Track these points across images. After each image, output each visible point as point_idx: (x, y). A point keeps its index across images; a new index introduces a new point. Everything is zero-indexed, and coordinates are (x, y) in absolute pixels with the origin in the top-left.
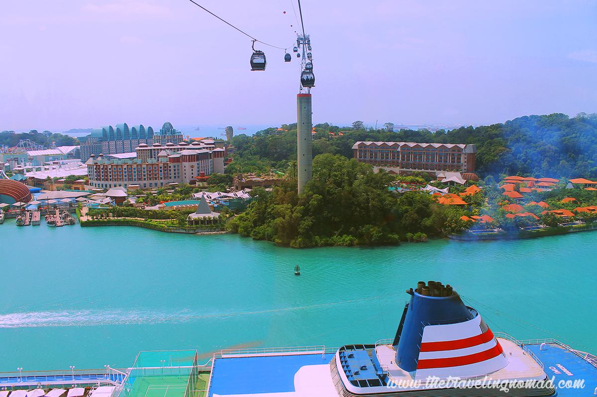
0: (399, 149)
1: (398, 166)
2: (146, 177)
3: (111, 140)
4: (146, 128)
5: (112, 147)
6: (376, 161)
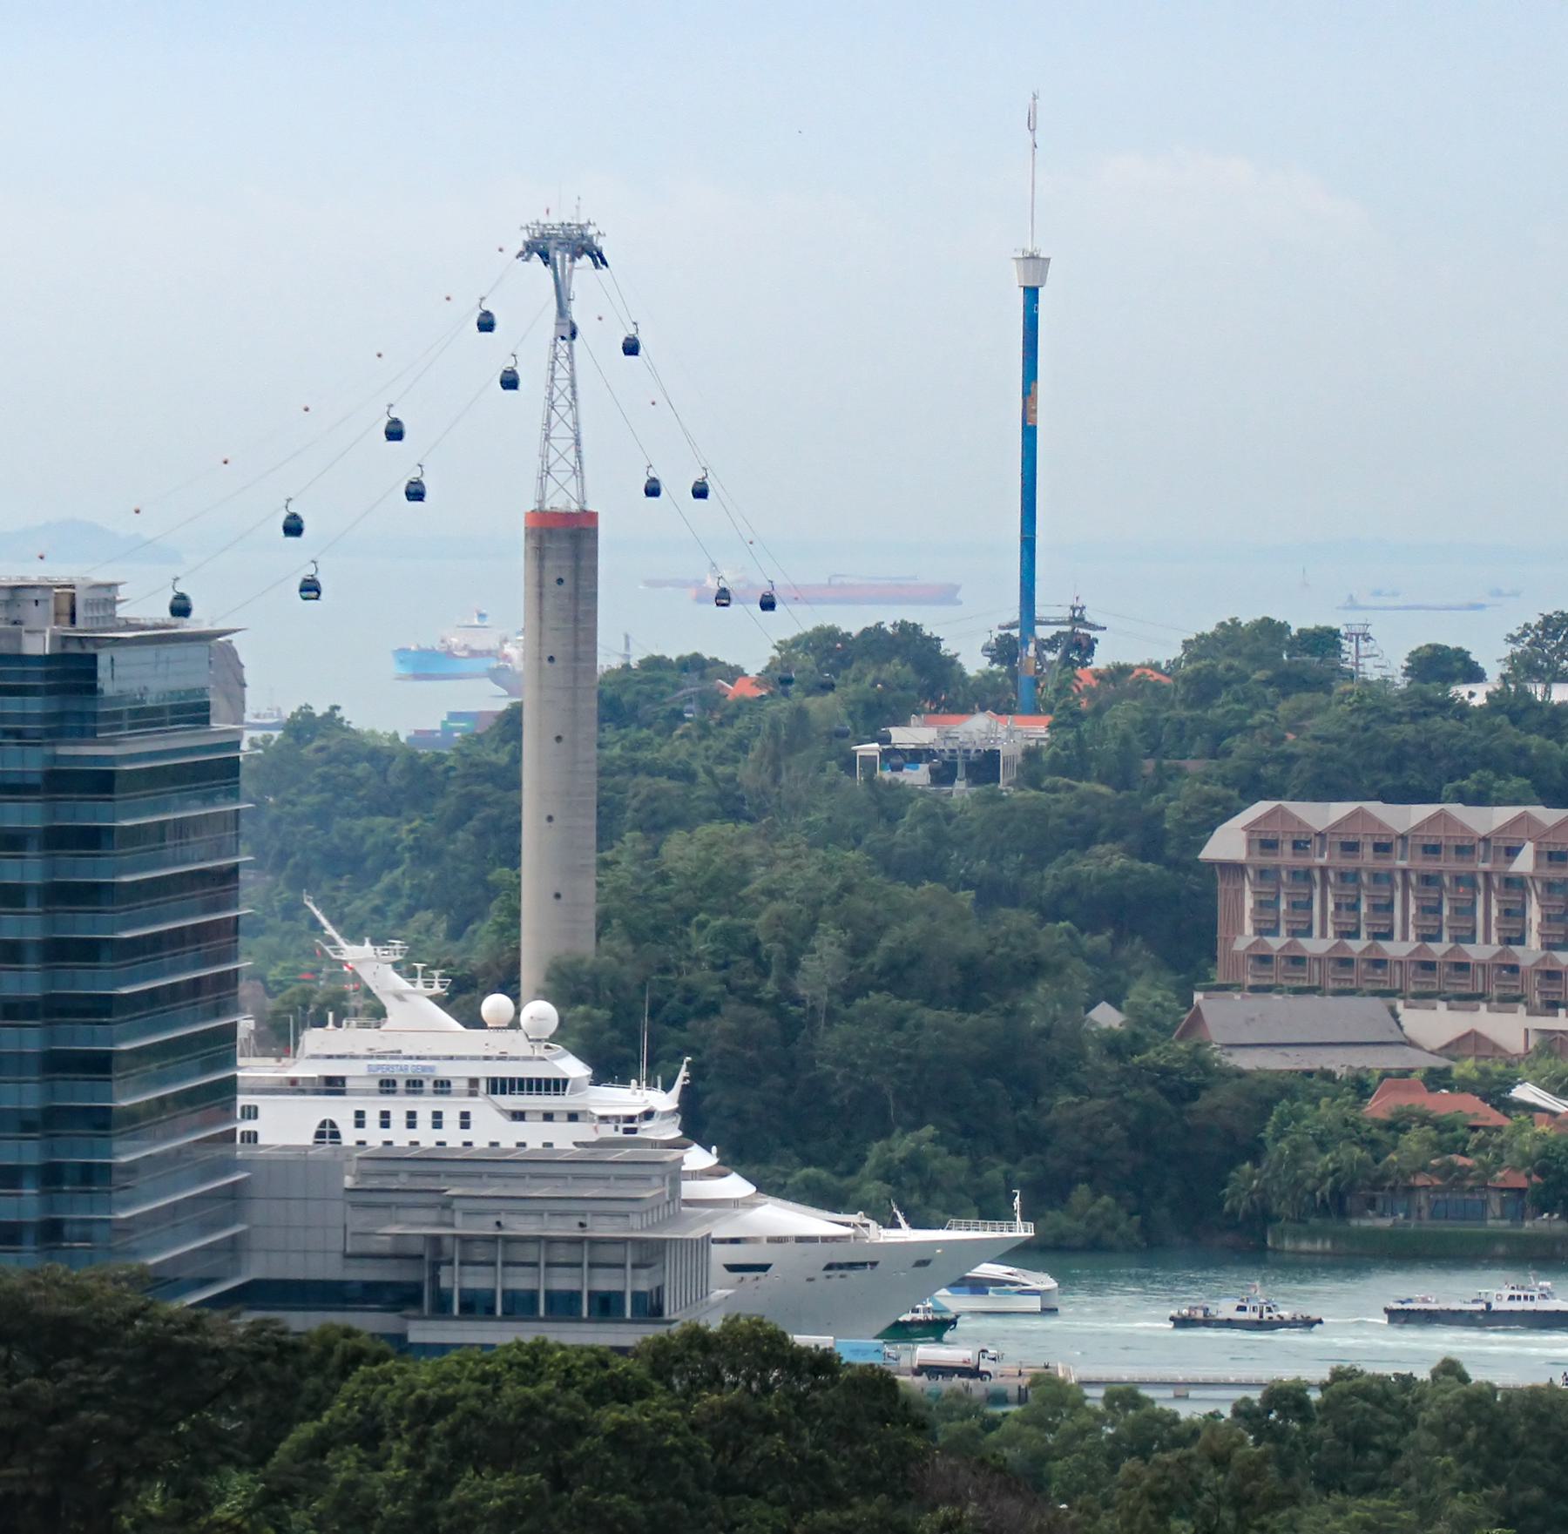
0: (1524, 863)
1: (1509, 1001)
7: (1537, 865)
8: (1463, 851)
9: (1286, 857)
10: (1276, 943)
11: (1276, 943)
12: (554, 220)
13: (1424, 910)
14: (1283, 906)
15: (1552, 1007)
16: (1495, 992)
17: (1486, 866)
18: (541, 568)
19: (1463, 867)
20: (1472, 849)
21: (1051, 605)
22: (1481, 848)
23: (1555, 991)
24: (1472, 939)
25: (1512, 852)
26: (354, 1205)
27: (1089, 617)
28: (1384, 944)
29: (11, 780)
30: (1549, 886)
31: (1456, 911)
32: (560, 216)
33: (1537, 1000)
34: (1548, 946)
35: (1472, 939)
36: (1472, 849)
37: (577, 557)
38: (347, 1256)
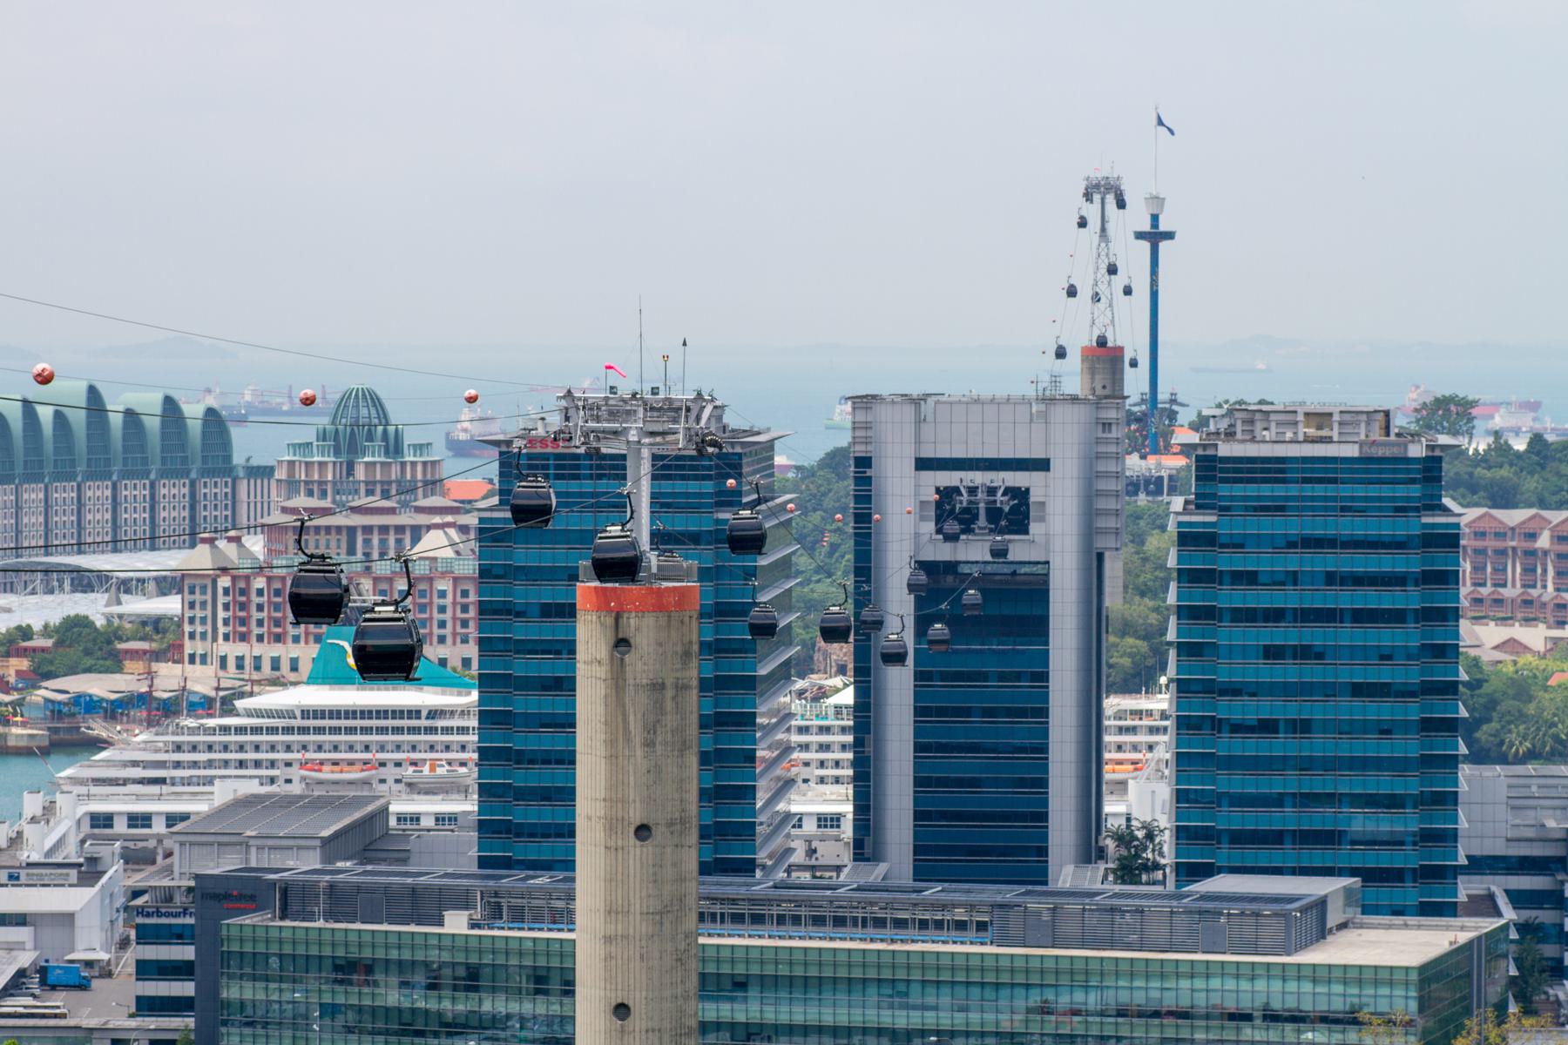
0: (1544, 541)
2: (448, 631)
3: (128, 474)
4: (193, 411)
5: (98, 518)
6: (1499, 602)
7: (1552, 543)
8: (1500, 535)
9: (1491, 544)
10: (1485, 591)
11: (1485, 591)
12: (1099, 175)
13: (1525, 570)
14: (1489, 569)
15: (1561, 624)
16: (1519, 615)
17: (1513, 544)
18: (1093, 379)
19: (1500, 544)
20: (1505, 534)
21: (1163, 395)
22: (1509, 534)
23: (1563, 614)
24: (1505, 585)
25: (1533, 536)
26: (1513, 808)
27: (1180, 398)
28: (1501, 590)
29: (1387, 540)
30: (1560, 556)
31: (1495, 570)
32: (1101, 172)
33: (1551, 620)
34: (1557, 590)
35: (1505, 585)
36: (1505, 534)
37: (1114, 373)
38: (1508, 840)
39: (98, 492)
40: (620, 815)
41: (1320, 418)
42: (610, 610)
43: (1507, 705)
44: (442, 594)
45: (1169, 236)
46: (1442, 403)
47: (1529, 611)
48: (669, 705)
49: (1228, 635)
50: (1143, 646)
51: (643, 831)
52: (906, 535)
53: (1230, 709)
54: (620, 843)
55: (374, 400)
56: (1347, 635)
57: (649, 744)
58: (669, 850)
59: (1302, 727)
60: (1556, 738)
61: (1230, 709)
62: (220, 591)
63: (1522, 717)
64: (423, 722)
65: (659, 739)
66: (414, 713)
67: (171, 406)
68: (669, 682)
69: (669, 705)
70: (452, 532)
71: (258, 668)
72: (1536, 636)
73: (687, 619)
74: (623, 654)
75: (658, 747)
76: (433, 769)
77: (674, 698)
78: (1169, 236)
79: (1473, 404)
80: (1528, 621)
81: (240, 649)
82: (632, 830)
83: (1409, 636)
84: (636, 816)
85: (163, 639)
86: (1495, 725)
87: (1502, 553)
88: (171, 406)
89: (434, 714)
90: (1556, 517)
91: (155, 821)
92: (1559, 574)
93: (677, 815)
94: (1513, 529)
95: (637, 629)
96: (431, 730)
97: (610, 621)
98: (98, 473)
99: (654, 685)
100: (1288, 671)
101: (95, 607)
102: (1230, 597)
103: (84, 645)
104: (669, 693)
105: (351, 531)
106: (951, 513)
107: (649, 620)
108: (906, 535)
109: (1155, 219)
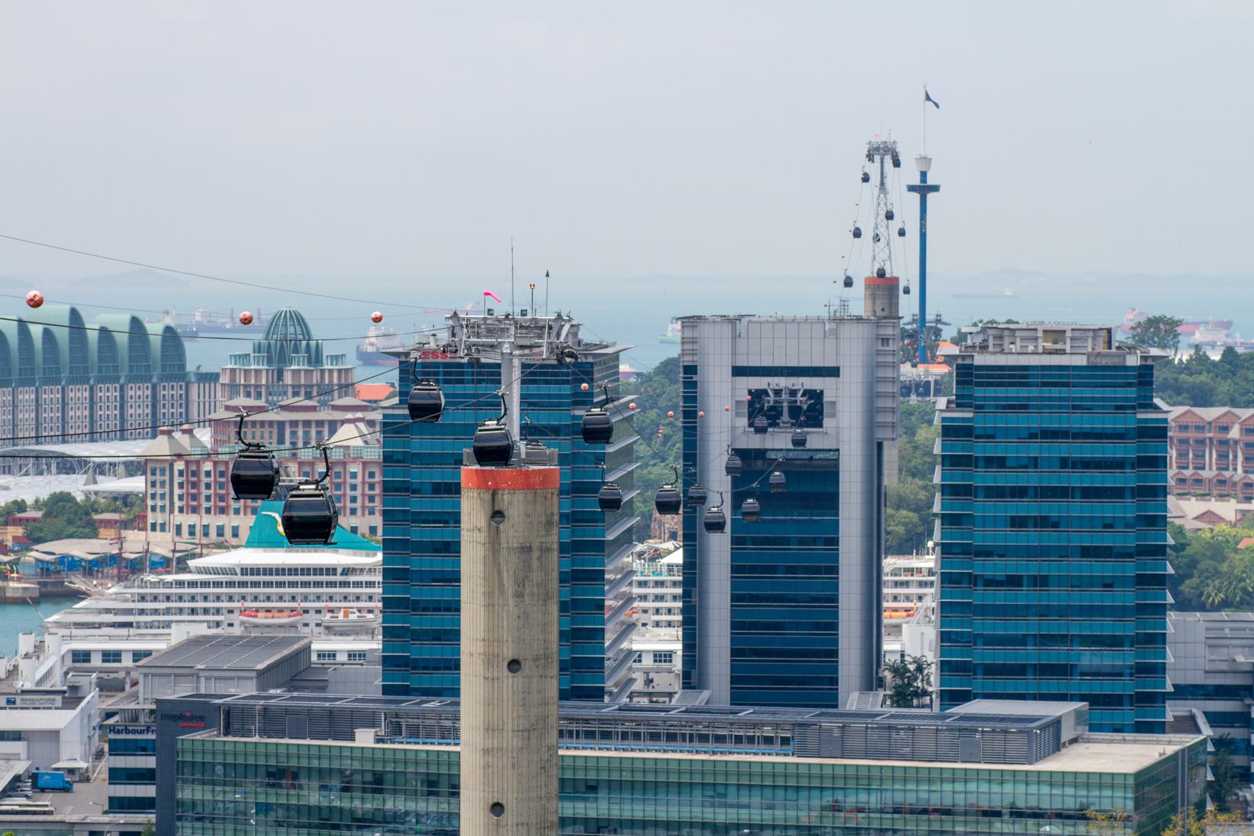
0: (1235, 433)
2: (358, 505)
3: (102, 379)
4: (154, 329)
5: (78, 415)
6: (1199, 481)
7: (1241, 434)
8: (1200, 428)
9: (1192, 435)
10: (1188, 473)
11: (1188, 473)
13: (1220, 456)
14: (1191, 455)
15: (1248, 499)
16: (1215, 492)
17: (1210, 435)
18: (874, 303)
19: (1200, 436)
20: (1204, 427)
21: (930, 316)
22: (1207, 427)
23: (1250, 491)
24: (1203, 468)
25: (1226, 429)
26: (1210, 646)
27: (944, 319)
28: (1200, 472)
29: (1109, 432)
30: (1247, 445)
31: (1195, 456)
33: (1241, 496)
34: (1245, 472)
35: (1203, 468)
36: (1204, 427)
37: (891, 299)
38: (1206, 672)
39: (78, 394)
40: (496, 652)
41: (1056, 335)
42: (488, 488)
43: (1205, 564)
44: (354, 475)
45: (935, 188)
46: (1153, 322)
47: (1223, 488)
48: (535, 564)
49: (982, 508)
50: (914, 517)
51: (514, 665)
52: (725, 428)
53: (983, 567)
54: (496, 674)
55: (299, 320)
56: (1077, 508)
57: (519, 595)
58: (535, 680)
59: (1042, 581)
60: (1244, 590)
61: (983, 567)
62: (176, 473)
63: (1217, 573)
64: (339, 578)
65: (527, 591)
66: (331, 571)
67: (136, 325)
68: (535, 545)
69: (535, 564)
70: (362, 425)
71: (206, 534)
72: (1228, 509)
73: (549, 496)
74: (499, 523)
75: (527, 598)
76: (346, 615)
77: (539, 558)
78: (935, 188)
79: (1178, 323)
80: (1222, 497)
81: (192, 519)
82: (505, 664)
83: (1127, 509)
84: (509, 653)
85: (130, 511)
86: (1195, 580)
87: (1201, 442)
88: (136, 325)
89: (347, 571)
90: (1244, 413)
91: (124, 656)
92: (1247, 459)
93: (542, 652)
94: (1210, 423)
95: (510, 503)
96: (345, 584)
97: (488, 496)
98: (78, 378)
99: (523, 548)
100: (1030, 537)
101: (76, 486)
102: (983, 478)
103: (67, 516)
104: (535, 554)
105: (281, 424)
106: (761, 410)
107: (519, 496)
108: (725, 428)
109: (924, 175)
